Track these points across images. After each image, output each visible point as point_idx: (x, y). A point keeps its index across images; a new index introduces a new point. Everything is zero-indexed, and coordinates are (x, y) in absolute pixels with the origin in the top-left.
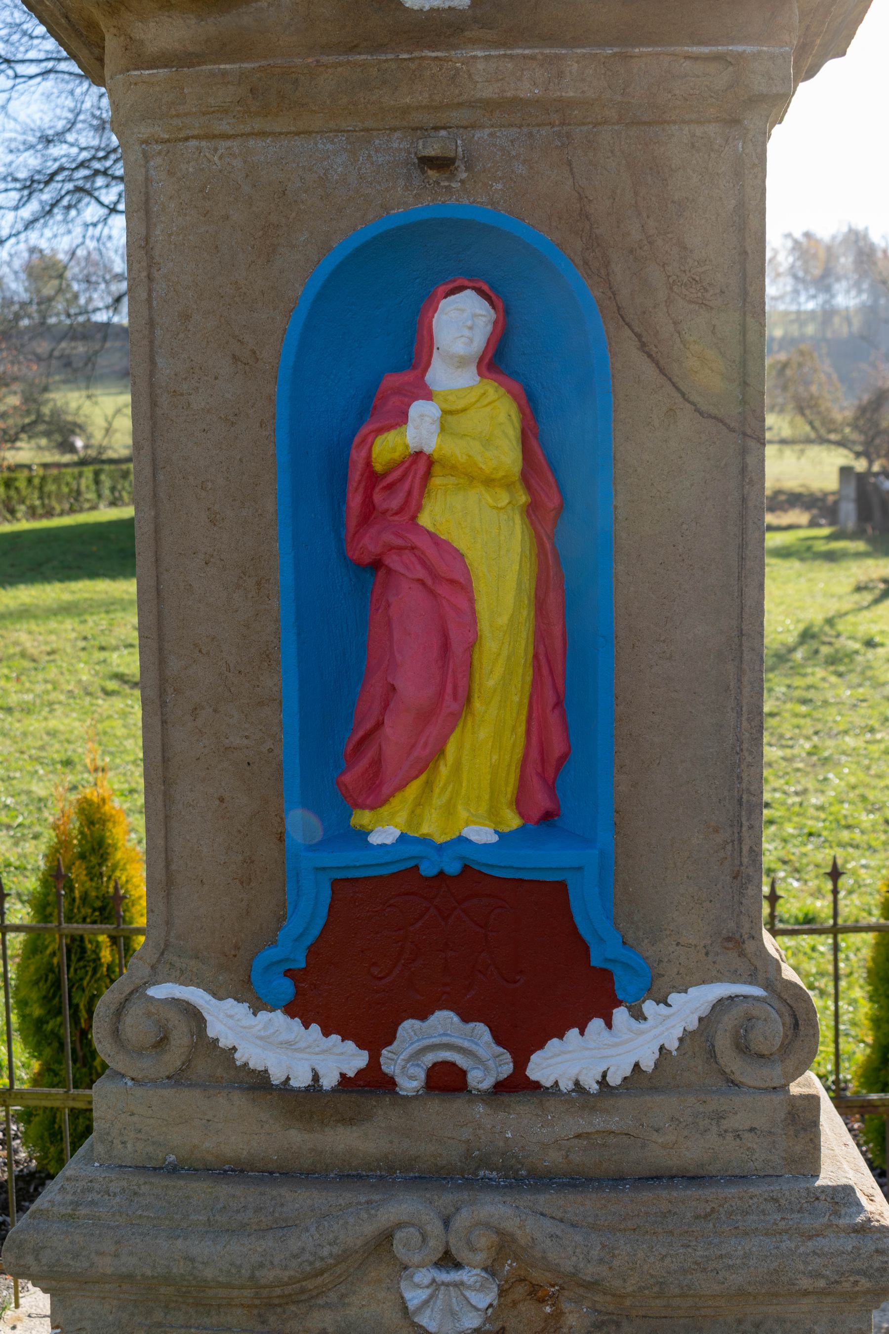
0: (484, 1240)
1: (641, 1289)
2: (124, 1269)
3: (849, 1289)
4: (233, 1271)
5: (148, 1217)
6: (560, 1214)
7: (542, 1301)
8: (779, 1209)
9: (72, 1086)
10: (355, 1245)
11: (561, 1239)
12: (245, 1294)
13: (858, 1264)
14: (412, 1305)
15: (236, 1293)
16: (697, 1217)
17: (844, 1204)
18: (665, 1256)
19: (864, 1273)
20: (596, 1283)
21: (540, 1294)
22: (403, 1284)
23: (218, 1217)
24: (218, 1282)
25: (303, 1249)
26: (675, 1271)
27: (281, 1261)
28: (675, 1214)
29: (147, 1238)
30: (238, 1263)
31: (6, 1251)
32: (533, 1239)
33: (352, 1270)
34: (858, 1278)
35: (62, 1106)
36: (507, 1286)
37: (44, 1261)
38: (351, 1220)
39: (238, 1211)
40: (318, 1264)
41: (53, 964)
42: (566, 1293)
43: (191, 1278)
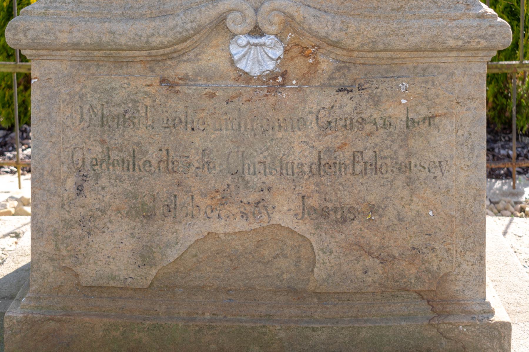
0: (277, 19)
1: (363, 45)
2: (75, 40)
3: (475, 47)
4: (137, 38)
5: (88, 13)
6: (319, 6)
7: (308, 56)
8: (438, 6)
9: (18, 60)
10: (205, 23)
11: (319, 17)
12: (143, 54)
13: (480, 33)
14: (236, 58)
15: (137, 53)
16: (393, 10)
17: (473, 5)
18: (376, 27)
19: (482, 37)
20: (338, 42)
21: (306, 52)
22: (231, 47)
23: (127, 11)
24: (128, 45)
25: (176, 25)
26: (382, 35)
27: (164, 32)
28: (381, 8)
29: (88, 23)
30: (140, 34)
31: (8, 31)
32: (304, 17)
33: (203, 39)
34: (480, 40)
35: (13, 71)
36: (288, 48)
37: (29, 37)
38: (203, 9)
39: (139, 8)
40: (184, 34)
41: (3, 6)
42: (321, 50)
43: (112, 44)
